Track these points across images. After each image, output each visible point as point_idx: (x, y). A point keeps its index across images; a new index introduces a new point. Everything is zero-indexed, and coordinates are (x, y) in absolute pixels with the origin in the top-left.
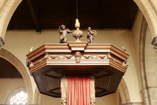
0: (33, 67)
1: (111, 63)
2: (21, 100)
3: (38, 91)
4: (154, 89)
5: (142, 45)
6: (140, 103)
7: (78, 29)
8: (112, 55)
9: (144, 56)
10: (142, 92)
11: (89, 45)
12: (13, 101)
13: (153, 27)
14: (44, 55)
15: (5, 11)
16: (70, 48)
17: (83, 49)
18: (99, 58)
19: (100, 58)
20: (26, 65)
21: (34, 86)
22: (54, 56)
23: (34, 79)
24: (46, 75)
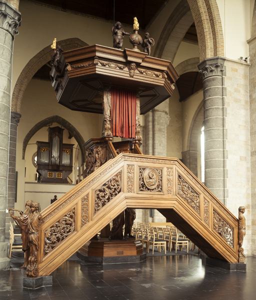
0: (170, 88)
4: (161, 113)
7: (137, 32)
8: (167, 74)
13: (205, 46)
14: (93, 58)
17: (139, 61)
18: (154, 76)
19: (118, 68)
22: (105, 62)
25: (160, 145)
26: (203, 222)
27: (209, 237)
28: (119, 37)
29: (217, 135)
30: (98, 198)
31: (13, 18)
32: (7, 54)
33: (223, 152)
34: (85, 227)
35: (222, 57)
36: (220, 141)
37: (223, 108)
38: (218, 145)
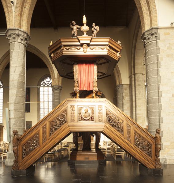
1: (109, 53)
2: (48, 83)
3: (59, 76)
5: (134, 41)
6: (128, 84)
7: (85, 25)
8: (110, 47)
9: (135, 49)
10: (130, 77)
11: (93, 39)
12: (42, 84)
14: (61, 47)
15: (26, 8)
16: (79, 42)
17: (88, 42)
19: (101, 49)
20: (49, 56)
21: (56, 72)
22: (68, 47)
23: (56, 69)
24: (63, 63)
25: (139, 94)
26: (126, 141)
27: (131, 150)
28: (75, 30)
29: (153, 81)
30: (52, 126)
31: (23, 36)
32: (21, 55)
33: (158, 93)
34: (45, 144)
35: (155, 27)
36: (155, 85)
37: (157, 62)
38: (154, 88)
